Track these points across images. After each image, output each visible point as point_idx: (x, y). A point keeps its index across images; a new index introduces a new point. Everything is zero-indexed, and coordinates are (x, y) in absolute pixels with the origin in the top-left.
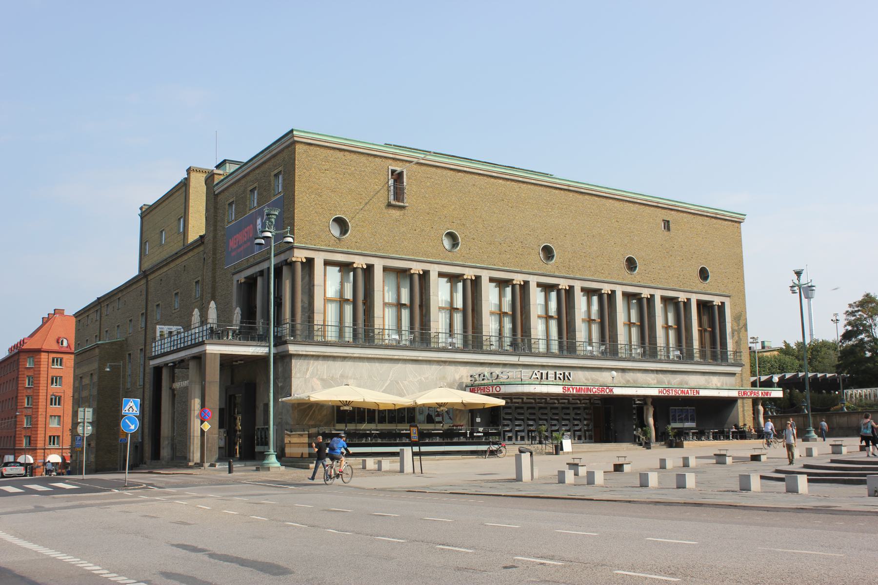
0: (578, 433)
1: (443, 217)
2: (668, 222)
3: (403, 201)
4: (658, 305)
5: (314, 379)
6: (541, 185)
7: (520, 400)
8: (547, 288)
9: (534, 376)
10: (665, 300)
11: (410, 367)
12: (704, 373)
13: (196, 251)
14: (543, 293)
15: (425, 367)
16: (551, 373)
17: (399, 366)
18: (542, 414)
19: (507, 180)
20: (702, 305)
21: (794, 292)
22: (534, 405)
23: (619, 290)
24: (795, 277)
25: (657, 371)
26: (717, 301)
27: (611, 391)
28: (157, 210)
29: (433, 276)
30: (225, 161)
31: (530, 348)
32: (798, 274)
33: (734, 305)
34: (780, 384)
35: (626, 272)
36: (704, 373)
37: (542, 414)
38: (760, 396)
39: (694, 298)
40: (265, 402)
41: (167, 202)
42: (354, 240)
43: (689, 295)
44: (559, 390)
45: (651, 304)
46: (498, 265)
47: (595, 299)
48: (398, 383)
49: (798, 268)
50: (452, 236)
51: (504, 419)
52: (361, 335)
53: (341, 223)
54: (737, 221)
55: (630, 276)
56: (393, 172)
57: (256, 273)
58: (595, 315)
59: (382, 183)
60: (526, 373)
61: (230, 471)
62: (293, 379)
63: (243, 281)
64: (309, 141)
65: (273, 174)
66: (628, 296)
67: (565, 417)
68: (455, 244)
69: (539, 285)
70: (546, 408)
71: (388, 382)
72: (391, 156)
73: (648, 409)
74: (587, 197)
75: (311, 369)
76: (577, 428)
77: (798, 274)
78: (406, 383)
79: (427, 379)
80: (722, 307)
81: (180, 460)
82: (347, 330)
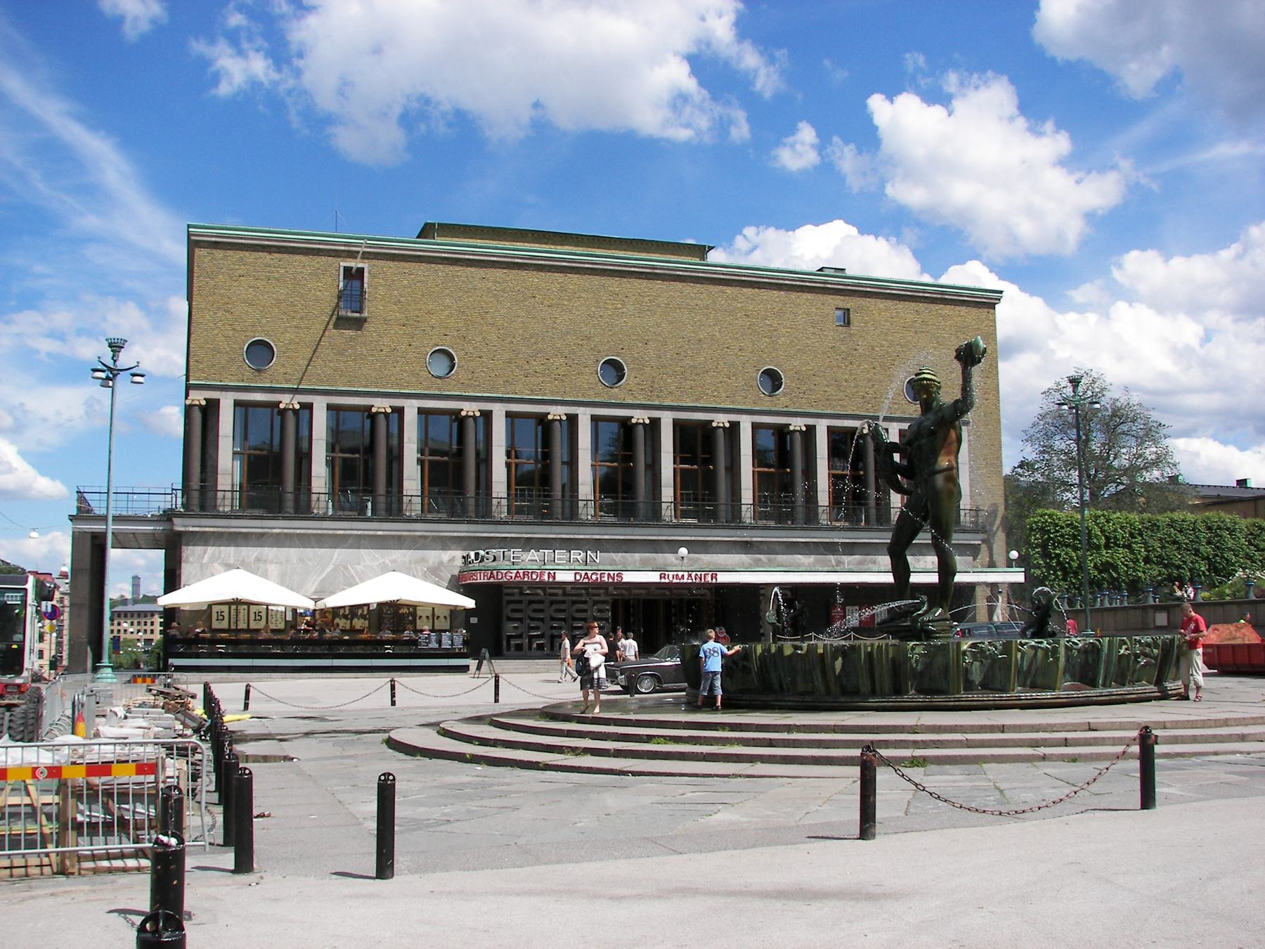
3: (360, 311)
5: (216, 565)
7: (560, 592)
18: (535, 611)
20: (839, 440)
22: (561, 598)
31: (400, 510)
35: (247, 368)
37: (535, 611)
42: (282, 370)
44: (653, 577)
46: (522, 393)
51: (510, 619)
52: (195, 501)
59: (324, 283)
62: (183, 565)
67: (578, 615)
70: (520, 602)
71: (331, 567)
78: (359, 568)
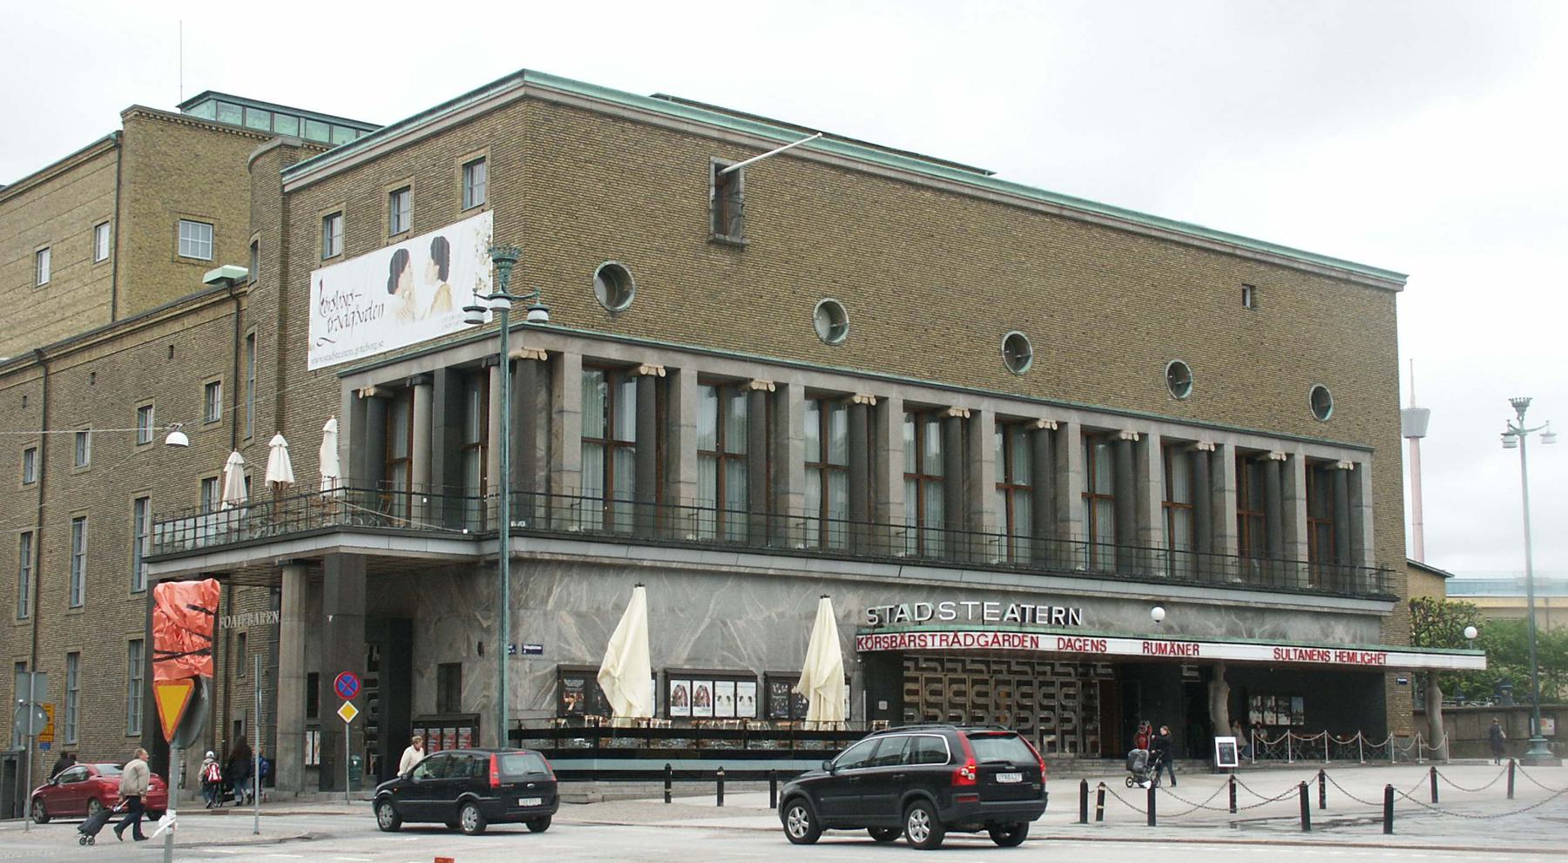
0: (1068, 738)
1: (815, 270)
2: (1252, 288)
4: (990, 442)
5: (563, 613)
6: (1007, 205)
8: (824, 402)
9: (1009, 615)
10: (1091, 436)
11: (749, 591)
12: (1317, 615)
13: (209, 315)
14: (713, 401)
15: (779, 590)
16: (1042, 609)
17: (727, 589)
19: (942, 191)
21: (1508, 445)
23: (989, 411)
24: (1514, 413)
25: (1228, 608)
26: (1345, 461)
27: (1035, 642)
28: (23, 199)
29: (796, 394)
30: (207, 93)
32: (1521, 406)
33: (1379, 472)
34: (1479, 643)
36: (1317, 615)
38: (1332, 660)
39: (1301, 453)
40: (447, 658)
41: (57, 183)
43: (1290, 447)
45: (1060, 445)
47: (933, 430)
48: (725, 624)
49: (1520, 395)
50: (831, 311)
53: (614, 278)
54: (1385, 287)
55: (1175, 404)
56: (719, 168)
57: (412, 378)
58: (1180, 496)
59: (698, 198)
60: (1212, 623)
61: (668, 798)
63: (372, 392)
64: (555, 98)
65: (461, 161)
66: (1006, 425)
68: (835, 332)
69: (703, 379)
71: (707, 621)
72: (715, 134)
73: (1217, 689)
74: (1095, 232)
75: (556, 591)
76: (1068, 727)
77: (1521, 406)
78: (741, 623)
79: (781, 615)
80: (1353, 474)
81: (1387, 757)
82: (931, 535)
